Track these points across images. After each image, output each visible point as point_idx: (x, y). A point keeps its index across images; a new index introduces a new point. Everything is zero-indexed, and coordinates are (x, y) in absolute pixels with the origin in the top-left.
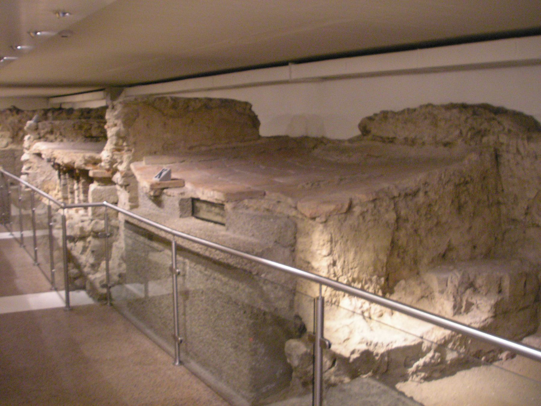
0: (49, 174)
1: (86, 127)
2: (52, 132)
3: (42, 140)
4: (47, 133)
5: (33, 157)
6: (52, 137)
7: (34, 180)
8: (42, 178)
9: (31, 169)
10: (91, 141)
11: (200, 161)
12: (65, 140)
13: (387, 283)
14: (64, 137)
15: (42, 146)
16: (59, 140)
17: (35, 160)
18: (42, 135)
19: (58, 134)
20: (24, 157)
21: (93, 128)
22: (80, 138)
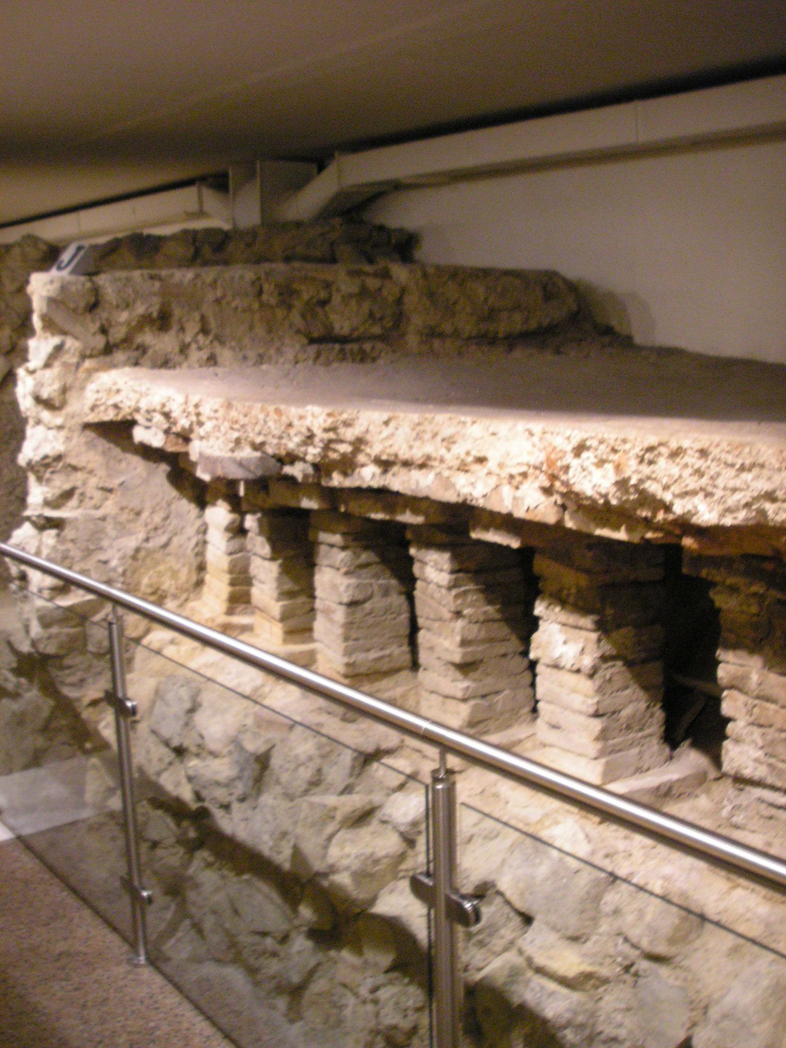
0: (157, 518)
1: (307, 293)
2: (162, 321)
3: (119, 356)
4: (146, 321)
5: (80, 439)
6: (166, 343)
7: (88, 553)
8: (131, 543)
9: (74, 502)
10: (343, 357)
11: (603, 346)
12: (225, 354)
13: (62, 397)
14: (220, 339)
15: (123, 387)
16: (195, 355)
17: (93, 456)
18: (118, 333)
19: (192, 328)
20: (37, 443)
21: (336, 299)
22: (292, 347)
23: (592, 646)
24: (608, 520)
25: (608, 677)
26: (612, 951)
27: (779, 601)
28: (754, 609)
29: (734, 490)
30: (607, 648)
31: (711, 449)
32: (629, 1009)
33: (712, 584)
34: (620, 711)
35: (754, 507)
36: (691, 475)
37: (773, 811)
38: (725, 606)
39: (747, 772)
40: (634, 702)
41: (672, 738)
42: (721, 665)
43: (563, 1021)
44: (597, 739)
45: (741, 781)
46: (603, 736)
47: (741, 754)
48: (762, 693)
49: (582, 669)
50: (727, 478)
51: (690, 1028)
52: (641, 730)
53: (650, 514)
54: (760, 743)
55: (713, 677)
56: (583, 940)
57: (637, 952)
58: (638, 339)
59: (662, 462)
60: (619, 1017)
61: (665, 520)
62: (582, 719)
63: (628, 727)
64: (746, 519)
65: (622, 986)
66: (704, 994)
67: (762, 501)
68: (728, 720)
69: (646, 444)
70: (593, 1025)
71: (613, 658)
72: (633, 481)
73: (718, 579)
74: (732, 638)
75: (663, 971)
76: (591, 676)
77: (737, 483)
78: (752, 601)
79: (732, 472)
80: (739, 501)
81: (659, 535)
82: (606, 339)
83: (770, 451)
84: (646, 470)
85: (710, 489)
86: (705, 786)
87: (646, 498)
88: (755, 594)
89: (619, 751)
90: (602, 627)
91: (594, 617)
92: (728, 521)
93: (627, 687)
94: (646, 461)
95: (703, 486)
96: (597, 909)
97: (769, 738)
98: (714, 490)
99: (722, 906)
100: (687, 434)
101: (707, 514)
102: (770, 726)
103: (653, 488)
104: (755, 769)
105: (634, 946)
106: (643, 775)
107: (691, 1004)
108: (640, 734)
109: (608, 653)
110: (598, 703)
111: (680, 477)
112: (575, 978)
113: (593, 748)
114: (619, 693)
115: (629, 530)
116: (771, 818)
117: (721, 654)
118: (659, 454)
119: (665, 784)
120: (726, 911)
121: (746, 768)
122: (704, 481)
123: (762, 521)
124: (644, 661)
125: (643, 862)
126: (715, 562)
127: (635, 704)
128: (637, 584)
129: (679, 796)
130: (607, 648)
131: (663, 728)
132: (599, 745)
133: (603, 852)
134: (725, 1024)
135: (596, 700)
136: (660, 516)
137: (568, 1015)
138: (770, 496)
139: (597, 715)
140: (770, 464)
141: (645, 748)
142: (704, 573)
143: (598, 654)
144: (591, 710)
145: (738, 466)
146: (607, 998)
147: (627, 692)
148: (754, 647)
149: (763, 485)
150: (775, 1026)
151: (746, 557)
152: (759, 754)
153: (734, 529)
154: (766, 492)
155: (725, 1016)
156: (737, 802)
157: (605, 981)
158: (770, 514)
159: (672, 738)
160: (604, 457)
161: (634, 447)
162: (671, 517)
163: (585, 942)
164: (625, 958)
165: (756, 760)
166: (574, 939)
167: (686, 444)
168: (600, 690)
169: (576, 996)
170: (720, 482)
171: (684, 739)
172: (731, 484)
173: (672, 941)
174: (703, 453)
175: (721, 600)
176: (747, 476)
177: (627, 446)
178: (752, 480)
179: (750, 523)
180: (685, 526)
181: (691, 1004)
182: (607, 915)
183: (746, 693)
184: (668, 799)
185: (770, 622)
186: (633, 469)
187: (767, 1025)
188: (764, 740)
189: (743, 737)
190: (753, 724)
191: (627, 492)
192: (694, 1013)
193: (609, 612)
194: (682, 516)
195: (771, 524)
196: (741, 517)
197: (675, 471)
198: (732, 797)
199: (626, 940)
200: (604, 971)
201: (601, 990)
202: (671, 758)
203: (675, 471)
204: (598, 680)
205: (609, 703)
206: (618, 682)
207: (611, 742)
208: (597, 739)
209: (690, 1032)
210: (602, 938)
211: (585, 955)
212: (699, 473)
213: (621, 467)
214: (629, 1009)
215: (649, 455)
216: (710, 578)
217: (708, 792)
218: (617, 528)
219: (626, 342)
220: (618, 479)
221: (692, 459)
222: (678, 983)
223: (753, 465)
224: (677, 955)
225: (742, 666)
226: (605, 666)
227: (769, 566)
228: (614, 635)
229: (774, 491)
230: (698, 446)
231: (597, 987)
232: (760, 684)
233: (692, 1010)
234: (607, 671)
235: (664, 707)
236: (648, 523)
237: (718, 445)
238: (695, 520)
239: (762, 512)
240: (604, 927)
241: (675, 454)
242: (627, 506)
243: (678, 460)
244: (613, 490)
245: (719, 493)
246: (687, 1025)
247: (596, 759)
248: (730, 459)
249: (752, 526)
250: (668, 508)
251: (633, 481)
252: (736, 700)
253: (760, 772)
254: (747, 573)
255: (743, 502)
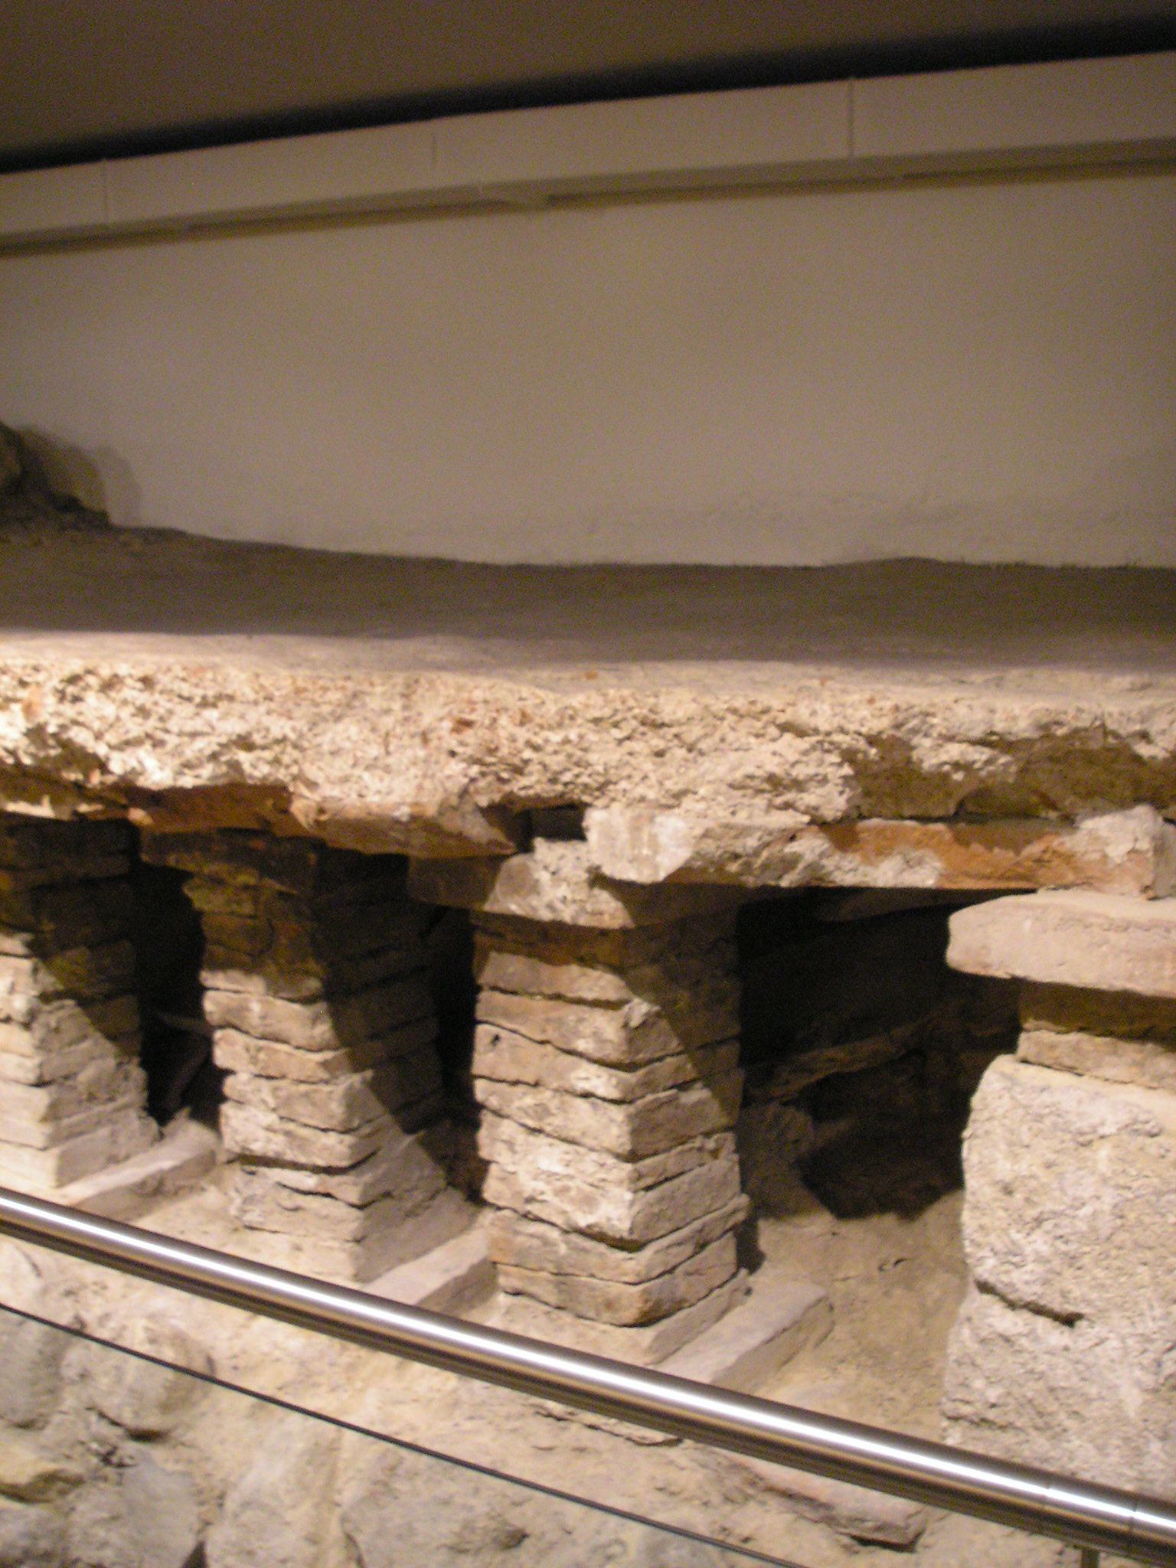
11: (63, 529)
23: (25, 980)
24: (24, 789)
25: (53, 1024)
26: (83, 1435)
27: (281, 894)
28: (247, 908)
29: (194, 735)
30: (49, 981)
31: (160, 676)
32: (115, 1518)
33: (184, 876)
34: (76, 1074)
35: (223, 759)
36: (133, 715)
37: (301, 1200)
38: (206, 908)
39: (257, 1148)
40: (96, 1059)
41: (160, 1109)
42: (210, 994)
43: (17, 1553)
44: (45, 1119)
45: (250, 1161)
46: (53, 1114)
47: (248, 1121)
48: (269, 1030)
49: (14, 1016)
50: (184, 718)
51: (199, 1532)
52: (112, 1099)
53: (80, 777)
54: (272, 1102)
55: (197, 1011)
56: (40, 1425)
57: (119, 1431)
58: (116, 518)
59: (91, 698)
60: (101, 1533)
61: (102, 783)
62: (20, 1091)
63: (92, 1097)
64: (214, 777)
65: (102, 1485)
66: (220, 1475)
67: (234, 749)
68: (227, 1072)
69: (67, 673)
70: (65, 1549)
71: (59, 995)
72: (52, 729)
73: (191, 867)
74: (219, 951)
75: (157, 1453)
76: (27, 1026)
77: (198, 725)
78: (244, 896)
79: (188, 709)
80: (201, 751)
81: (98, 807)
82: (69, 518)
83: (243, 676)
84: (69, 710)
85: (159, 735)
86: (214, 1173)
87: (73, 753)
88: (246, 887)
89: (81, 1134)
90: (39, 951)
91: (28, 936)
92: (188, 781)
93: (85, 1037)
94: (69, 698)
95: (150, 731)
96: (57, 1375)
97: (282, 1094)
98: (166, 737)
99: (237, 1345)
100: (126, 655)
101: (157, 773)
102: (283, 1077)
103: (80, 736)
104: (269, 1141)
105: (115, 1423)
106: (121, 1166)
107: (199, 1496)
108: (110, 1106)
109: (51, 989)
110: (41, 1065)
111: (118, 719)
112: (31, 1486)
113: (38, 1133)
114: (73, 1048)
115: (54, 803)
116: (296, 1209)
117: (208, 978)
118: (88, 687)
119: (152, 1176)
120: (244, 1352)
121: (256, 1140)
122: (151, 724)
123: (237, 778)
124: (108, 997)
125: (124, 1296)
126: (185, 842)
127: (100, 1062)
128: (89, 882)
129: (176, 1193)
130: (49, 981)
131: (145, 1095)
132: (48, 1129)
133: (62, 1288)
134: (248, 1516)
135: (37, 1060)
136: (96, 778)
137: (25, 1543)
138: (245, 743)
139: (40, 1084)
140: (243, 695)
141: (120, 1126)
142: (172, 860)
143: (35, 993)
144: (32, 1077)
145: (198, 700)
146: (82, 1507)
147: (86, 1045)
148: (251, 965)
149: (234, 727)
150: (317, 1506)
151: (230, 833)
152: (272, 1119)
153: (197, 791)
154: (240, 736)
155: (246, 1505)
156: (247, 1192)
157: (77, 1482)
158: (247, 768)
159: (160, 1109)
160: (10, 694)
161: (50, 678)
162: (110, 779)
163: (42, 1428)
164: (102, 1441)
165: (269, 1129)
166: (26, 1426)
167: (123, 669)
168: (42, 1046)
169: (34, 1512)
170: (173, 725)
171: (180, 1107)
172: (189, 726)
173: (165, 1407)
174: (147, 682)
175: (201, 898)
176: (211, 714)
177: (41, 677)
178: (219, 719)
179: (221, 782)
180: (129, 791)
181: (199, 1496)
182: (73, 1382)
183: (246, 1033)
184: (160, 1198)
185: (270, 925)
186: (51, 709)
187: (306, 1507)
188: (276, 1097)
189: (250, 1096)
190: (259, 1076)
191: (45, 745)
192: (203, 1509)
193: (48, 926)
194: (123, 778)
195: (250, 782)
196: (205, 774)
197: (110, 710)
198: (240, 1185)
199: (102, 1415)
200: (74, 1468)
201: (71, 1497)
202: (161, 1136)
203: (110, 710)
204: (39, 1031)
205: (56, 1064)
206: (70, 1030)
207: (66, 1121)
208: (45, 1119)
209: (201, 1537)
210: (68, 1421)
211: (44, 1448)
212: (143, 712)
213: (34, 708)
214: (115, 1518)
215: (71, 689)
216: (181, 867)
217: (218, 1182)
218: (35, 801)
219: (98, 522)
220: (30, 726)
221: (132, 692)
222: (179, 1467)
223: (220, 697)
224: (176, 1427)
225: (236, 992)
226: (47, 1008)
227: (258, 844)
228: (58, 961)
229: (249, 734)
230: (139, 673)
231: (63, 1493)
232: (263, 1017)
233: (202, 1503)
234: (51, 1016)
235: (143, 1064)
236: (80, 790)
237: (169, 670)
238: (142, 782)
239: (235, 766)
240: (70, 1400)
241: (109, 685)
242: (48, 766)
243: (113, 694)
244: (23, 743)
245: (172, 740)
246: (197, 1526)
247: (44, 1149)
248: (186, 689)
249: (224, 787)
250: (103, 767)
251: (52, 729)
252: (232, 1044)
253: (274, 1145)
254: (229, 857)
255: (208, 752)
